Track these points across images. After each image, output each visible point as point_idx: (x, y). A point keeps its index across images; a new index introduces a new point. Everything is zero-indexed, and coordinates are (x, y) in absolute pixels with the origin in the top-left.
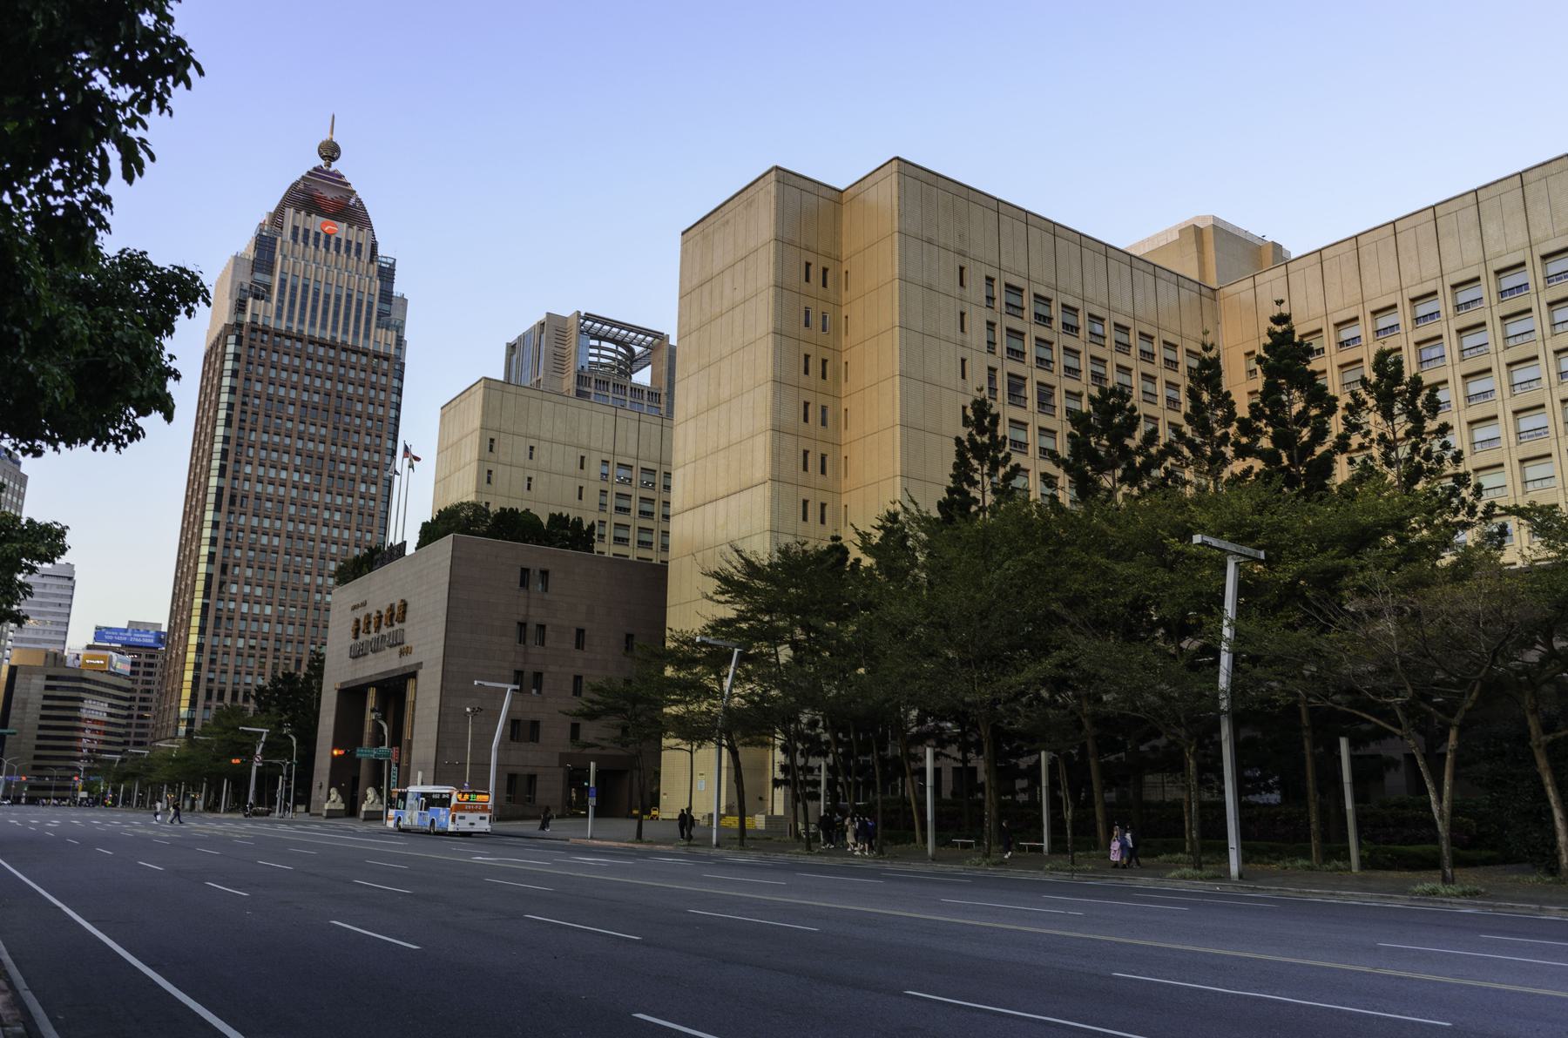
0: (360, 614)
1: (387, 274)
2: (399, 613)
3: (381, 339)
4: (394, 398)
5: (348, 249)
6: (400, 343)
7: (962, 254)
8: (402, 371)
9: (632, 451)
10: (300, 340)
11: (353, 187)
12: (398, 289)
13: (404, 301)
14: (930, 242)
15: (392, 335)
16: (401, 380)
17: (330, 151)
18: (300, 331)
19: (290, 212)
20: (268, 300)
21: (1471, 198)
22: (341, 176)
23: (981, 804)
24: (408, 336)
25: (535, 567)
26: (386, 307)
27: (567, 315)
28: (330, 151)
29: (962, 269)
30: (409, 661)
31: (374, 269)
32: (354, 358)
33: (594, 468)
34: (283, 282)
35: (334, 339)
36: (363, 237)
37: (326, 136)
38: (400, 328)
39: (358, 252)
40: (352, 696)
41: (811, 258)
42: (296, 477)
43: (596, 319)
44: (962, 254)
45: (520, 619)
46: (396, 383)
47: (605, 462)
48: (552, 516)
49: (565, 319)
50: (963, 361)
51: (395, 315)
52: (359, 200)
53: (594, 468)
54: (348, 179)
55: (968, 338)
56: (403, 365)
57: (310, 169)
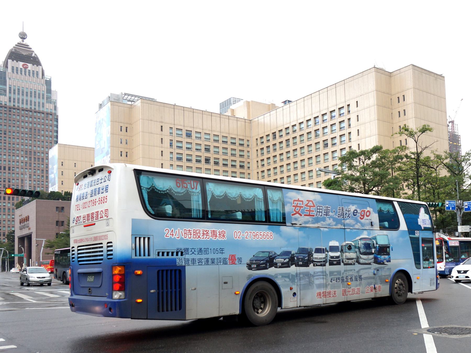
0: (20, 218)
1: (48, 83)
2: (27, 219)
3: (48, 107)
4: (55, 129)
5: (33, 74)
6: (55, 108)
7: (162, 122)
8: (57, 119)
9: (182, 123)
10: (19, 109)
11: (33, 49)
12: (53, 88)
13: (56, 92)
14: (151, 120)
15: (52, 106)
16: (57, 122)
17: (23, 36)
18: (18, 106)
19: (10, 61)
20: (5, 95)
21: (334, 86)
22: (28, 46)
23: (14, 257)
24: (58, 105)
25: (61, 206)
26: (49, 95)
27: (118, 94)
28: (23, 36)
29: (162, 126)
30: (30, 231)
31: (43, 81)
32: (39, 115)
33: (166, 130)
34: (10, 88)
35: (31, 108)
36: (39, 69)
37: (21, 31)
38: (55, 103)
39: (37, 74)
40: (21, 239)
41: (122, 125)
42: (22, 159)
43: (129, 95)
44: (162, 122)
45: (57, 220)
46: (55, 123)
47: (171, 128)
48: (65, 192)
49: (118, 95)
50: (162, 151)
51: (53, 98)
52: (35, 54)
53: (166, 130)
54: (30, 46)
55: (163, 144)
56: (58, 116)
57: (16, 43)
